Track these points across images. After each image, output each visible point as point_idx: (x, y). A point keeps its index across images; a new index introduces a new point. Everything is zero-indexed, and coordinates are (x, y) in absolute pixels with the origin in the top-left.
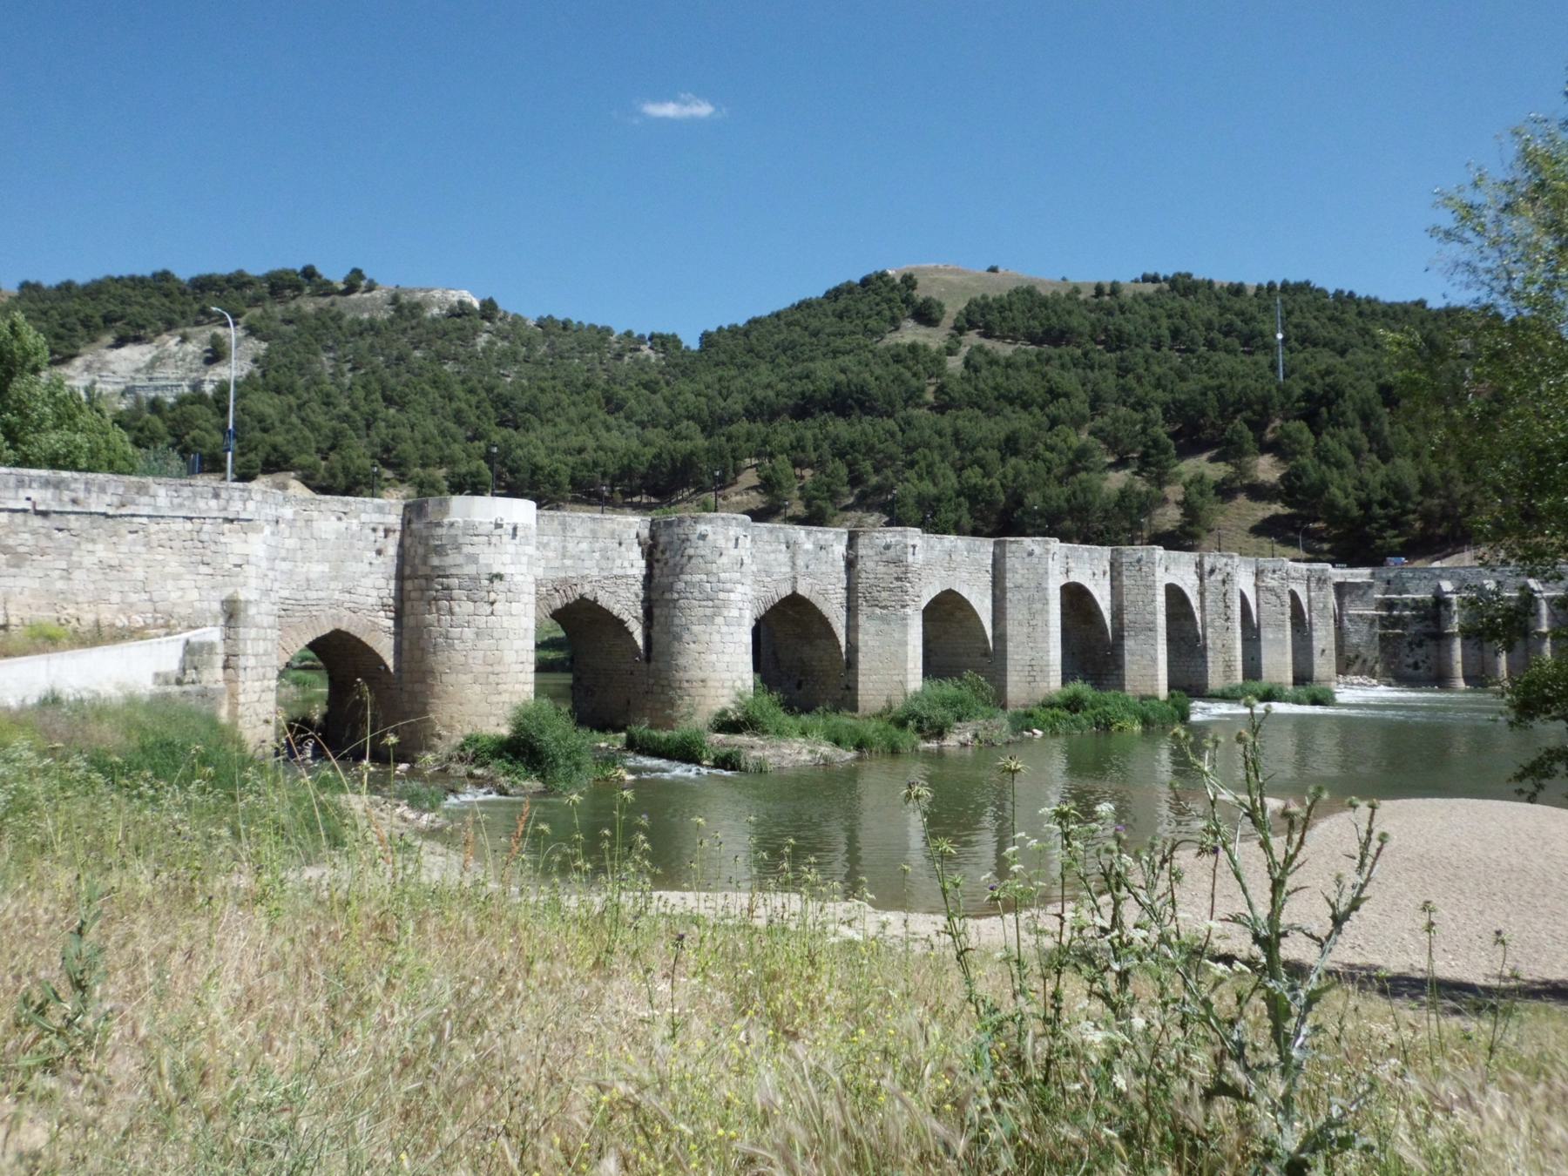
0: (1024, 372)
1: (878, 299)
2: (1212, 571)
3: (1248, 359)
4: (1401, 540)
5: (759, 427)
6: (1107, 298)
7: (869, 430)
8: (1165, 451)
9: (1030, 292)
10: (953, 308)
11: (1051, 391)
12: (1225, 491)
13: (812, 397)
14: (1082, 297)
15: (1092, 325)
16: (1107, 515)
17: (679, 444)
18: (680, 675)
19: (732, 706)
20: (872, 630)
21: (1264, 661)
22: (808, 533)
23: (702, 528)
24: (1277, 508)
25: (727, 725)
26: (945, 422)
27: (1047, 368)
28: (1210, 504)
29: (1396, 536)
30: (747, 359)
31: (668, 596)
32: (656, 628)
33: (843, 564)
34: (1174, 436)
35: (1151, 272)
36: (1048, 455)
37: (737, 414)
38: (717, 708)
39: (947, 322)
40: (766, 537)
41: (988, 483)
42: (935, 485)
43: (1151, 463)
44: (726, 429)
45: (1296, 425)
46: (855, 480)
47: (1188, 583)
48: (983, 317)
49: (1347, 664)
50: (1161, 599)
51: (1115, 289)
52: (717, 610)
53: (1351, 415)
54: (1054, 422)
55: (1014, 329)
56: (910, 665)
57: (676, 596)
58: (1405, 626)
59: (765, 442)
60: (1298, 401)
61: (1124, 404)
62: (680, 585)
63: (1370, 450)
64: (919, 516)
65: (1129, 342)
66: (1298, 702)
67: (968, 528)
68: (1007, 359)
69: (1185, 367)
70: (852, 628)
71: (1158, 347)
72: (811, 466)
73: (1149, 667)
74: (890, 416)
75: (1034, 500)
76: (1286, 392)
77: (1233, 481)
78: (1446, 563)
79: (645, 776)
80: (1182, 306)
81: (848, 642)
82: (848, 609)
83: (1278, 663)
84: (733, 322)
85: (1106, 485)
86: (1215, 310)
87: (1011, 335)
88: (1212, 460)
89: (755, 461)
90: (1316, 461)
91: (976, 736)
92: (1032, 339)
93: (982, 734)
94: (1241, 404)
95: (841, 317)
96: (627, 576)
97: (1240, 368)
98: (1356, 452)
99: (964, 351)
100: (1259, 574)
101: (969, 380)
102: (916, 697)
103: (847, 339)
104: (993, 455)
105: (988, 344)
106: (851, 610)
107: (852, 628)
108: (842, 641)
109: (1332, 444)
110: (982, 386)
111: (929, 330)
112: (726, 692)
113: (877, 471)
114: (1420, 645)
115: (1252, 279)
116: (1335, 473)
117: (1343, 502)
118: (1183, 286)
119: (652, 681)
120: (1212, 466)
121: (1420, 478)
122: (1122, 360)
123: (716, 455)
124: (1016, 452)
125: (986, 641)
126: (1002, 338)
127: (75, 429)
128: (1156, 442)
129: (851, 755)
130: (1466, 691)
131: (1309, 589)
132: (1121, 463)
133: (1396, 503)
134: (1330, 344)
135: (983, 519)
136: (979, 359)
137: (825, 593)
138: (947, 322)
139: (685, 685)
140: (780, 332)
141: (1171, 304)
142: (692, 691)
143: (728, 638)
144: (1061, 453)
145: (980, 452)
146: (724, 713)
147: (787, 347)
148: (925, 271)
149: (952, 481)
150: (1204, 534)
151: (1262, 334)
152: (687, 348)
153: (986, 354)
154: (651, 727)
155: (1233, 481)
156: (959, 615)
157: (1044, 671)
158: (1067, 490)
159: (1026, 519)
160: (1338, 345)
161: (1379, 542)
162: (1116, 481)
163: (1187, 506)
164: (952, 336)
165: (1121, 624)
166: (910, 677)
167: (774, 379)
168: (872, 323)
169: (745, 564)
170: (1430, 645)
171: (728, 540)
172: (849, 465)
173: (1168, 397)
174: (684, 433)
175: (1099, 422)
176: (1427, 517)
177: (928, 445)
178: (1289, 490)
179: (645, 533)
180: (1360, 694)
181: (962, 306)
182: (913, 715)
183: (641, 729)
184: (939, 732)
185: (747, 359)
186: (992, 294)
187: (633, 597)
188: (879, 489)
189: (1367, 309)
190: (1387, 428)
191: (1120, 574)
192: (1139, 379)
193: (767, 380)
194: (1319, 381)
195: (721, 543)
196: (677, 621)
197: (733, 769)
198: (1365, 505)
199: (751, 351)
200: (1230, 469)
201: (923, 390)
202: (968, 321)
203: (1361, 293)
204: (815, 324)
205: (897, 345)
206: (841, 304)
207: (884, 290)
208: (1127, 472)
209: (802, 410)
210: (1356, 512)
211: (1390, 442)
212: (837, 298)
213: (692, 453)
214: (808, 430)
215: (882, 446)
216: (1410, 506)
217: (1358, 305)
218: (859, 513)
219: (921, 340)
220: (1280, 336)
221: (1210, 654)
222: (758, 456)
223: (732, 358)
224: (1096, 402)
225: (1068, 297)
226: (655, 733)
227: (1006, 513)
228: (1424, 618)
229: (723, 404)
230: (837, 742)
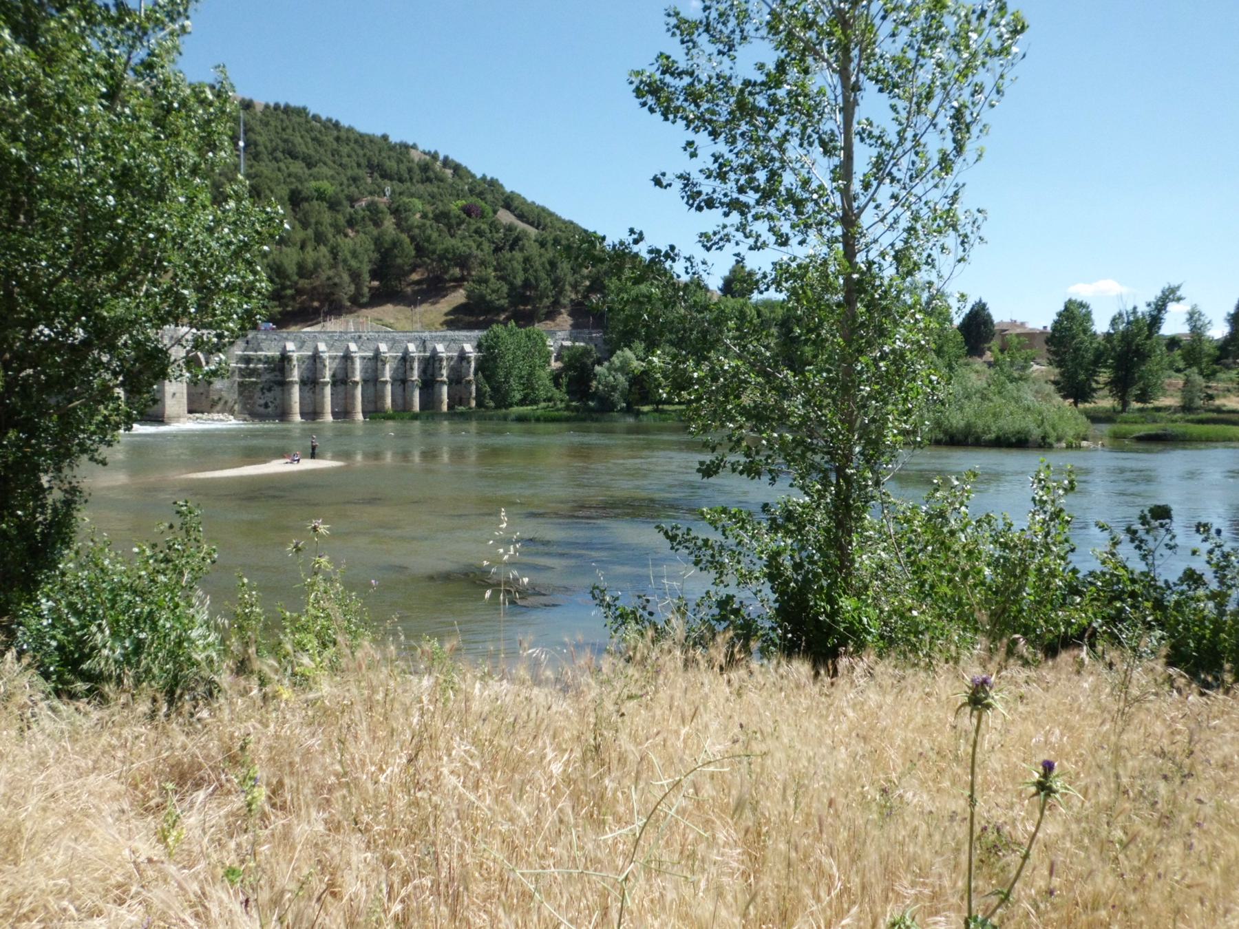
58: (259, 375)
78: (317, 328)
84: (330, 116)
114: (270, 390)
170: (277, 389)
203: (345, 123)
228: (273, 370)
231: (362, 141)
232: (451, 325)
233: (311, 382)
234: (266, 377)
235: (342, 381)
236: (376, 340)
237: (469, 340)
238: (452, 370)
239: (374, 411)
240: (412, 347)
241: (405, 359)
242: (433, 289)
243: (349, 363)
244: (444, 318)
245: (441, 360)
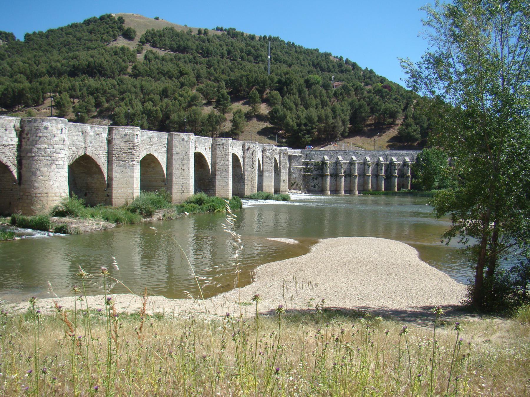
0: (169, 63)
1: (108, 26)
2: (248, 149)
3: (256, 65)
4: (311, 139)
5: (54, 79)
6: (202, 35)
7: (104, 83)
8: (227, 100)
9: (172, 29)
10: (140, 33)
11: (180, 72)
12: (248, 117)
13: (78, 67)
14: (193, 34)
15: (197, 46)
16: (203, 124)
17: (16, 84)
18: (36, 191)
19: (60, 205)
20: (119, 171)
21: (264, 184)
22: (92, 128)
23: (45, 124)
24: (267, 125)
25: (59, 213)
26: (137, 82)
27: (178, 62)
28: (243, 122)
29: (309, 138)
30: (47, 48)
31: (29, 154)
32: (24, 169)
33: (106, 141)
34: (230, 93)
35: (220, 26)
36: (180, 98)
37: (43, 73)
38: (53, 206)
39: (137, 39)
40: (73, 129)
41: (155, 109)
42: (133, 108)
43: (220, 104)
44: (40, 79)
45: (275, 93)
46: (98, 105)
47: (240, 154)
48: (152, 38)
49: (291, 186)
50: (231, 160)
52: (53, 161)
53: (295, 90)
54: (182, 85)
55: (165, 45)
56: (135, 186)
57: (33, 155)
58: (312, 172)
59: (57, 86)
60: (276, 83)
61: (210, 79)
62: (36, 150)
63: (301, 104)
64: (126, 122)
65: (211, 54)
66: (277, 199)
67: (147, 127)
68: (163, 57)
69: (233, 66)
70: (110, 170)
71: (222, 57)
72: (78, 98)
73: (225, 186)
74: (113, 78)
75: (174, 116)
76: (272, 80)
77: (251, 113)
78: (326, 148)
79: (24, 237)
81: (108, 176)
82: (108, 162)
83: (269, 186)
84: (41, 30)
85: (203, 112)
86: (245, 45)
87: (164, 47)
88: (243, 104)
89: (52, 94)
90: (282, 107)
91: (164, 216)
92: (172, 49)
93: (167, 215)
94: (256, 82)
95: (91, 33)
96: (10, 145)
97: (254, 68)
98: (296, 105)
99: (144, 52)
100: (264, 151)
101: (147, 65)
102: (137, 200)
103: (93, 42)
104: (157, 97)
105: (154, 50)
106: (110, 162)
107: (110, 170)
108: (106, 175)
109: (288, 101)
110: (152, 67)
111: (130, 42)
112: (57, 198)
113: (107, 101)
114: (316, 179)
115: (258, 34)
116: (289, 112)
117: (291, 124)
118: (232, 33)
119: (22, 194)
120: (244, 106)
121: (318, 116)
122: (209, 61)
123: (34, 91)
124: (167, 97)
125: (164, 176)
126: (160, 48)
128: (223, 95)
129: (114, 225)
130: (345, 196)
131: (280, 158)
132: (209, 103)
133: (310, 125)
134: (285, 62)
135: (153, 124)
136: (151, 56)
137: (98, 154)
138: (137, 39)
139: (38, 195)
140: (63, 37)
141: (227, 40)
142: (42, 198)
143: (58, 174)
144: (185, 98)
145: (152, 96)
146: (57, 208)
147: (66, 44)
148: (128, 16)
149: (139, 107)
150: (240, 133)
151: (261, 56)
152: (18, 40)
153: (154, 54)
154: (24, 214)
155: (251, 113)
156: (153, 164)
157: (187, 188)
158: (187, 113)
159: (171, 125)
160: (288, 63)
161: (303, 139)
162: (207, 110)
163: (234, 121)
164: (139, 45)
165: (215, 169)
166: (135, 191)
167: (60, 58)
168: (105, 37)
169: (65, 140)
170: (320, 178)
171: (58, 130)
172: (95, 98)
173: (228, 78)
174: (19, 80)
175: (201, 86)
176: (319, 130)
177: (130, 91)
178: (273, 117)
179: (18, 125)
180: (298, 197)
181: (144, 33)
182: (138, 207)
183: (19, 216)
184: (149, 214)
185: (47, 48)
187: (12, 155)
188: (108, 109)
190: (307, 96)
191: (215, 149)
192: (215, 70)
193: (58, 59)
194: (284, 76)
195: (55, 131)
196: (34, 166)
197: (64, 233)
198: (299, 125)
199: (49, 44)
200: (250, 108)
201: (127, 68)
202: (146, 39)
203: (297, 44)
204: (79, 35)
206: (91, 27)
207: (111, 23)
208: (211, 107)
209: (73, 73)
210: (296, 128)
211: (308, 102)
212: (89, 24)
213: (23, 89)
214: (77, 82)
215: (109, 91)
216: (314, 126)
217: (296, 48)
218: (99, 119)
219: (126, 46)
220: (269, 57)
221: (246, 181)
222: (54, 92)
223: (40, 47)
224: (198, 77)
225: (188, 33)
226: (26, 217)
227: (163, 121)
228: (318, 169)
229: (37, 68)
230: (107, 219)
231: (309, 53)
232: (392, 147)
233: (335, 175)
234: (315, 173)
235: (349, 175)
236: (365, 155)
237: (407, 156)
238: (399, 170)
239: (363, 190)
240: (381, 159)
241: (378, 164)
242: (378, 129)
243: (352, 166)
244: (387, 144)
245: (395, 165)
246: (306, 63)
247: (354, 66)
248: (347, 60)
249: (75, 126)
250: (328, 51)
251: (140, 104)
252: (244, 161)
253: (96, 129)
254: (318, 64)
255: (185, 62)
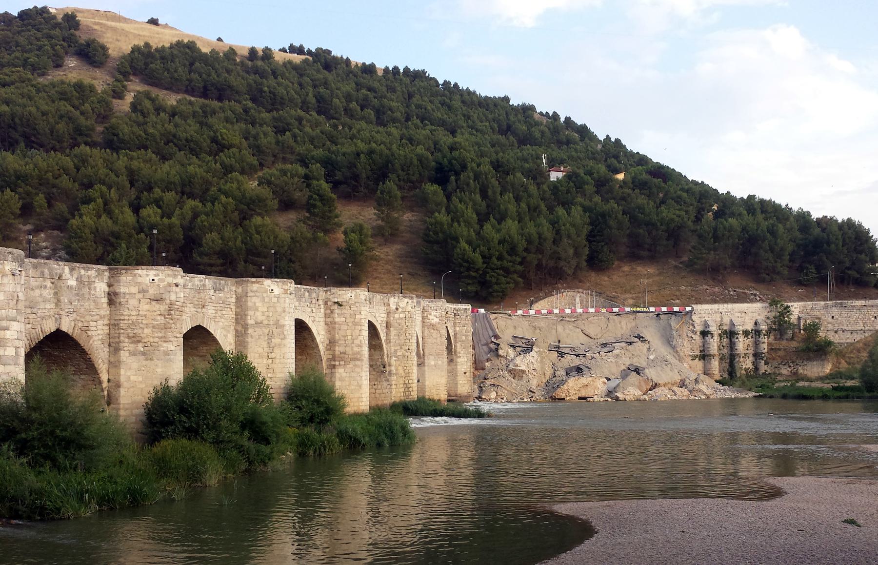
1: (39, 35)
20: (135, 365)
22: (72, 270)
26: (121, 161)
35: (297, 44)
40: (31, 272)
51: (267, 54)
54: (227, 170)
65: (282, 104)
70: (115, 365)
75: (211, 239)
80: (326, 79)
87: (171, 87)
92: (190, 90)
105: (155, 92)
106: (114, 348)
118: (324, 60)
127: (37, 45)
136: (147, 104)
145: (157, 192)
149: (129, 217)
186: (155, 44)
189: (467, 97)
198: (486, 258)
203: (463, 85)
205: (63, 82)
217: (462, 95)
219: (87, 81)
246: (484, 125)
247: (583, 131)
248: (407, 70)
249: (35, 267)
250: (529, 101)
251: (128, 211)
252: (388, 334)
253: (83, 272)
254: (509, 127)
255: (227, 120)
